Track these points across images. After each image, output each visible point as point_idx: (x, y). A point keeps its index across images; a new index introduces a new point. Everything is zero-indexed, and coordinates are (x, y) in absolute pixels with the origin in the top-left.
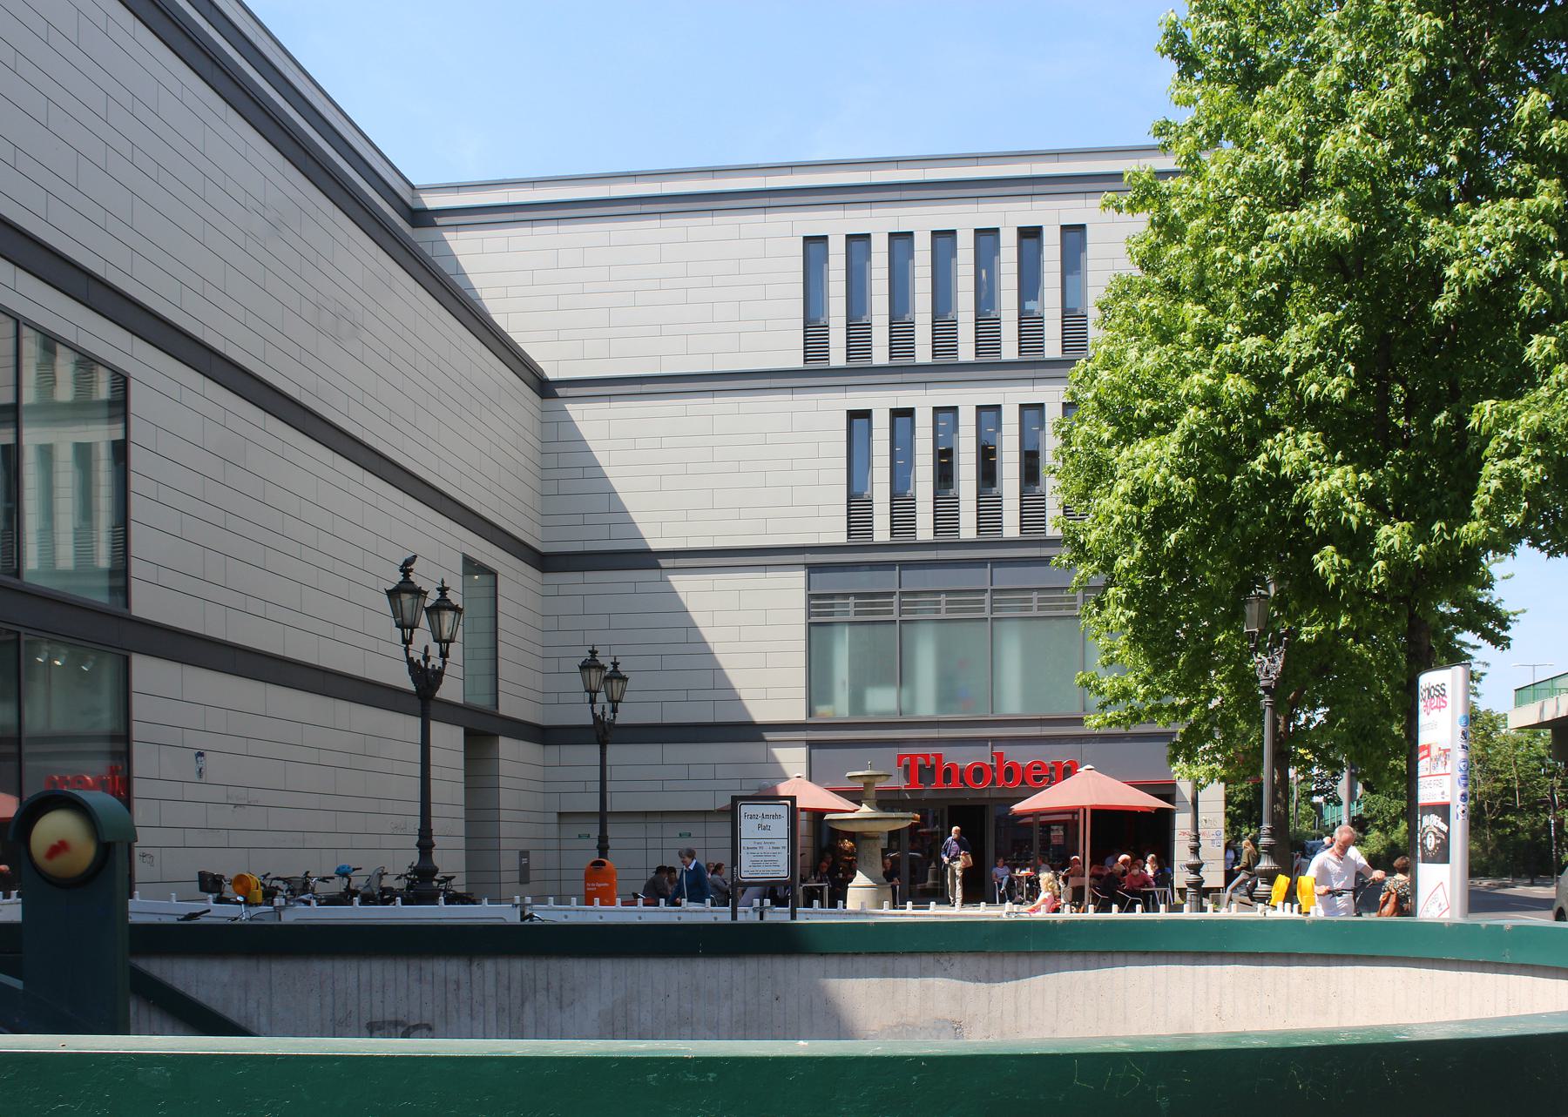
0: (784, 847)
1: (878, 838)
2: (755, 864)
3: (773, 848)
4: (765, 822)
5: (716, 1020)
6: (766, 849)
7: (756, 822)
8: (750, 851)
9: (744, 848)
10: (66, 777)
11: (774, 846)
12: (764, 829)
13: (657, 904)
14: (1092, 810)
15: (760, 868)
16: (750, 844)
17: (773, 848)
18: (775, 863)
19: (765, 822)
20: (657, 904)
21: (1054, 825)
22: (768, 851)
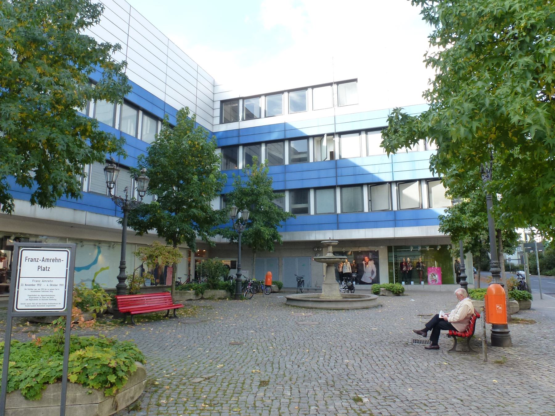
0: (61, 285)
1: (59, 317)
2: (31, 298)
3: (51, 285)
4: (44, 265)
5: (9, 264)
6: (44, 285)
7: (35, 265)
8: (27, 287)
9: (22, 285)
10: (406, 284)
11: (52, 283)
12: (44, 270)
13: (420, 283)
14: (296, 203)
15: (35, 302)
16: (29, 281)
17: (51, 285)
18: (52, 297)
19: (44, 265)
20: (420, 283)
21: (220, 245)
22: (47, 288)
